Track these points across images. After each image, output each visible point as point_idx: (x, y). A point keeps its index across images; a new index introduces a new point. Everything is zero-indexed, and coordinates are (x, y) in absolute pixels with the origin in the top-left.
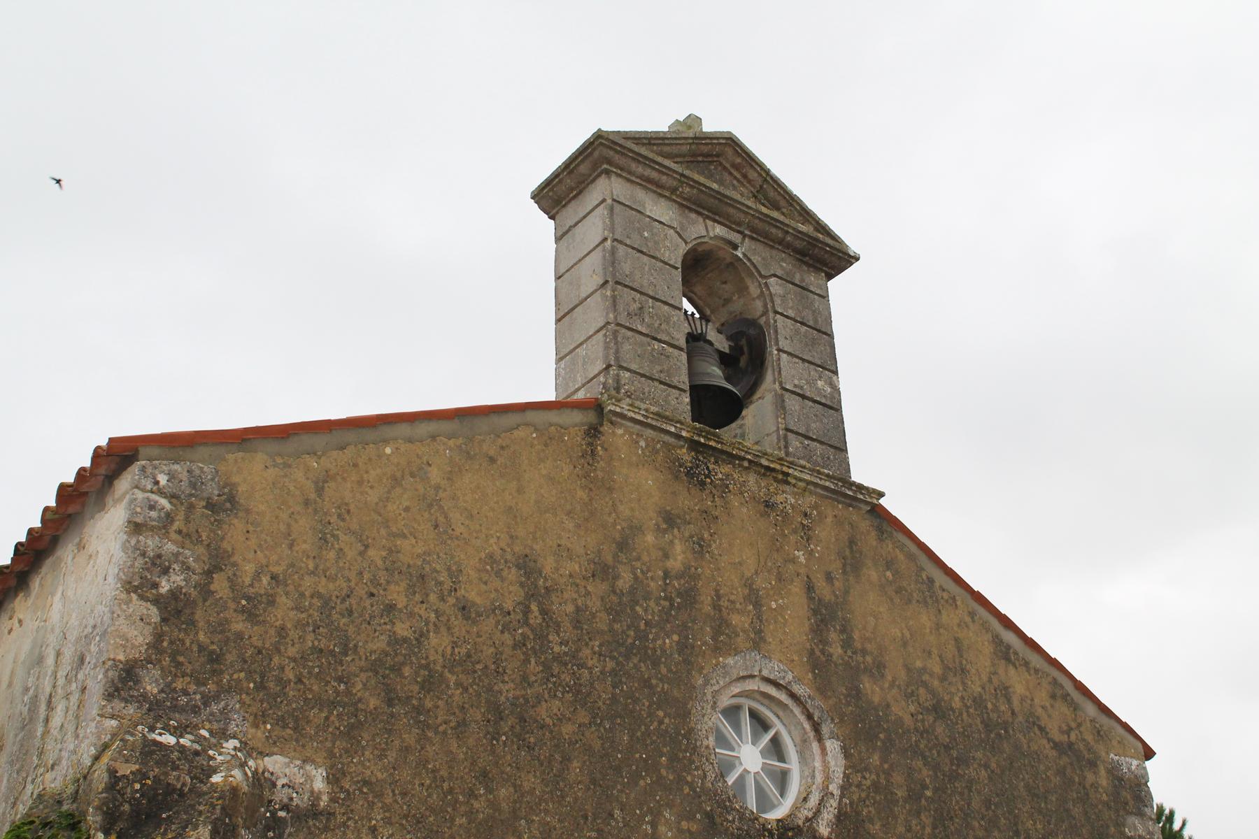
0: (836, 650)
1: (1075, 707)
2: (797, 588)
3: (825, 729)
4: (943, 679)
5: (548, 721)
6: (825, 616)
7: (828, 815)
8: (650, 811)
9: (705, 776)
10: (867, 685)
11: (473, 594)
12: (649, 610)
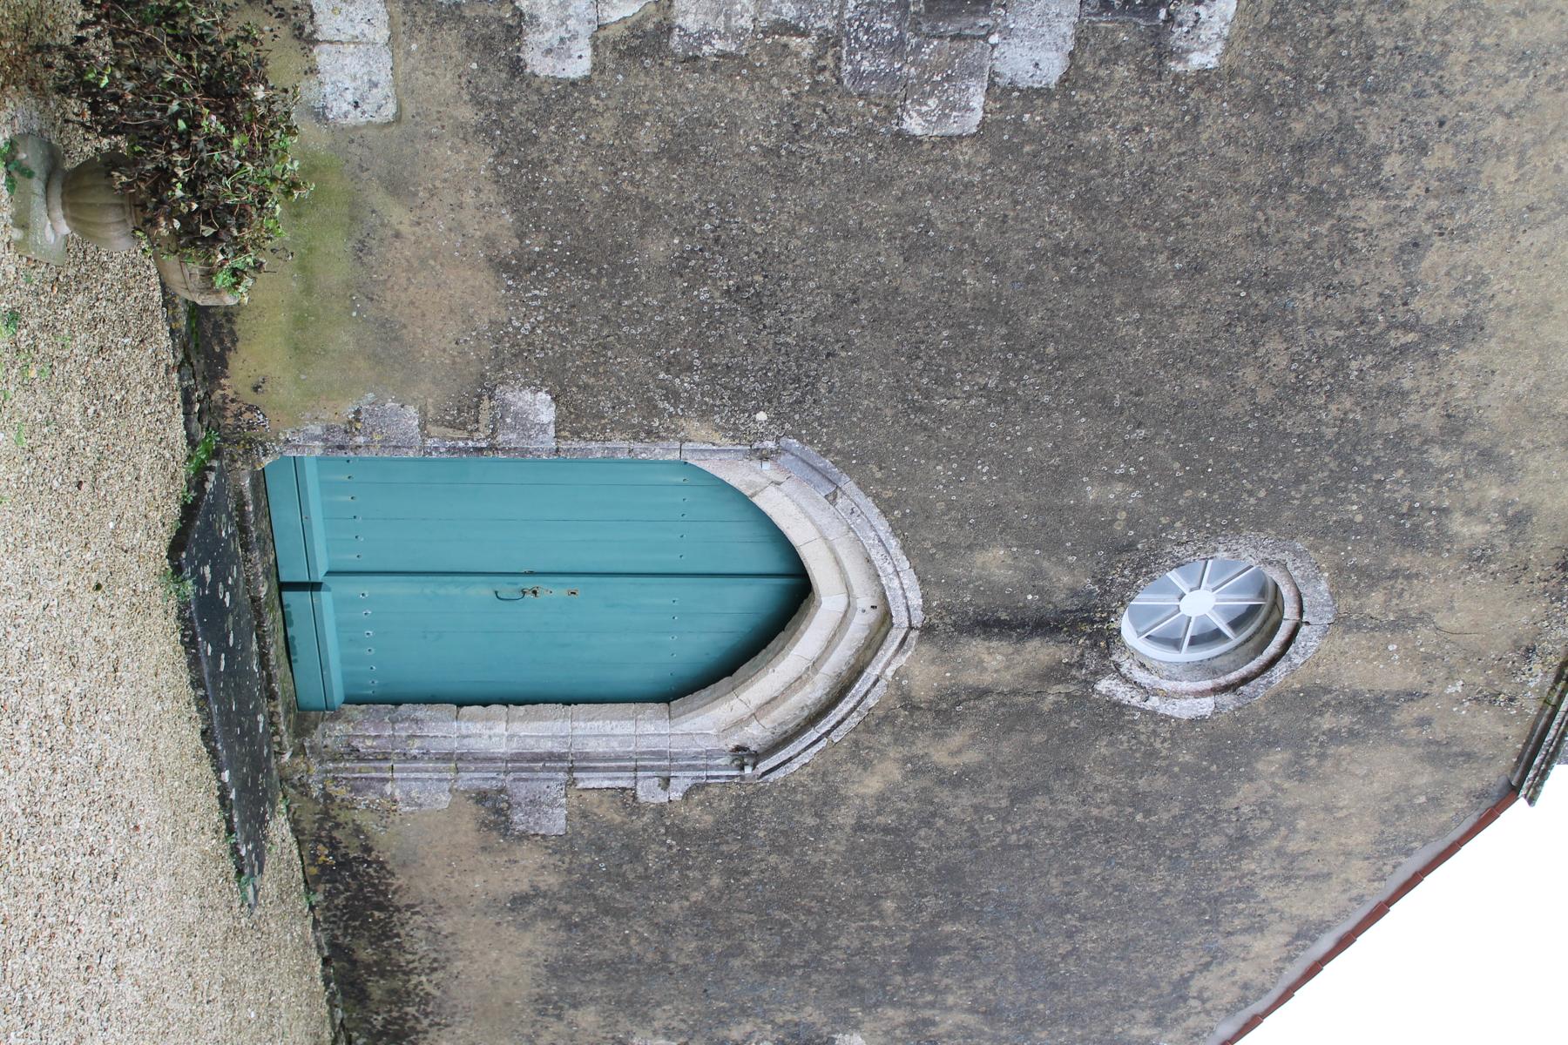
0: (1327, 722)
1: (1230, 1011)
2: (1412, 679)
3: (1227, 699)
4: (1280, 852)
6: (1373, 712)
7: (1122, 692)
8: (1141, 474)
10: (1279, 756)
11: (1434, 258)
12: (1398, 486)
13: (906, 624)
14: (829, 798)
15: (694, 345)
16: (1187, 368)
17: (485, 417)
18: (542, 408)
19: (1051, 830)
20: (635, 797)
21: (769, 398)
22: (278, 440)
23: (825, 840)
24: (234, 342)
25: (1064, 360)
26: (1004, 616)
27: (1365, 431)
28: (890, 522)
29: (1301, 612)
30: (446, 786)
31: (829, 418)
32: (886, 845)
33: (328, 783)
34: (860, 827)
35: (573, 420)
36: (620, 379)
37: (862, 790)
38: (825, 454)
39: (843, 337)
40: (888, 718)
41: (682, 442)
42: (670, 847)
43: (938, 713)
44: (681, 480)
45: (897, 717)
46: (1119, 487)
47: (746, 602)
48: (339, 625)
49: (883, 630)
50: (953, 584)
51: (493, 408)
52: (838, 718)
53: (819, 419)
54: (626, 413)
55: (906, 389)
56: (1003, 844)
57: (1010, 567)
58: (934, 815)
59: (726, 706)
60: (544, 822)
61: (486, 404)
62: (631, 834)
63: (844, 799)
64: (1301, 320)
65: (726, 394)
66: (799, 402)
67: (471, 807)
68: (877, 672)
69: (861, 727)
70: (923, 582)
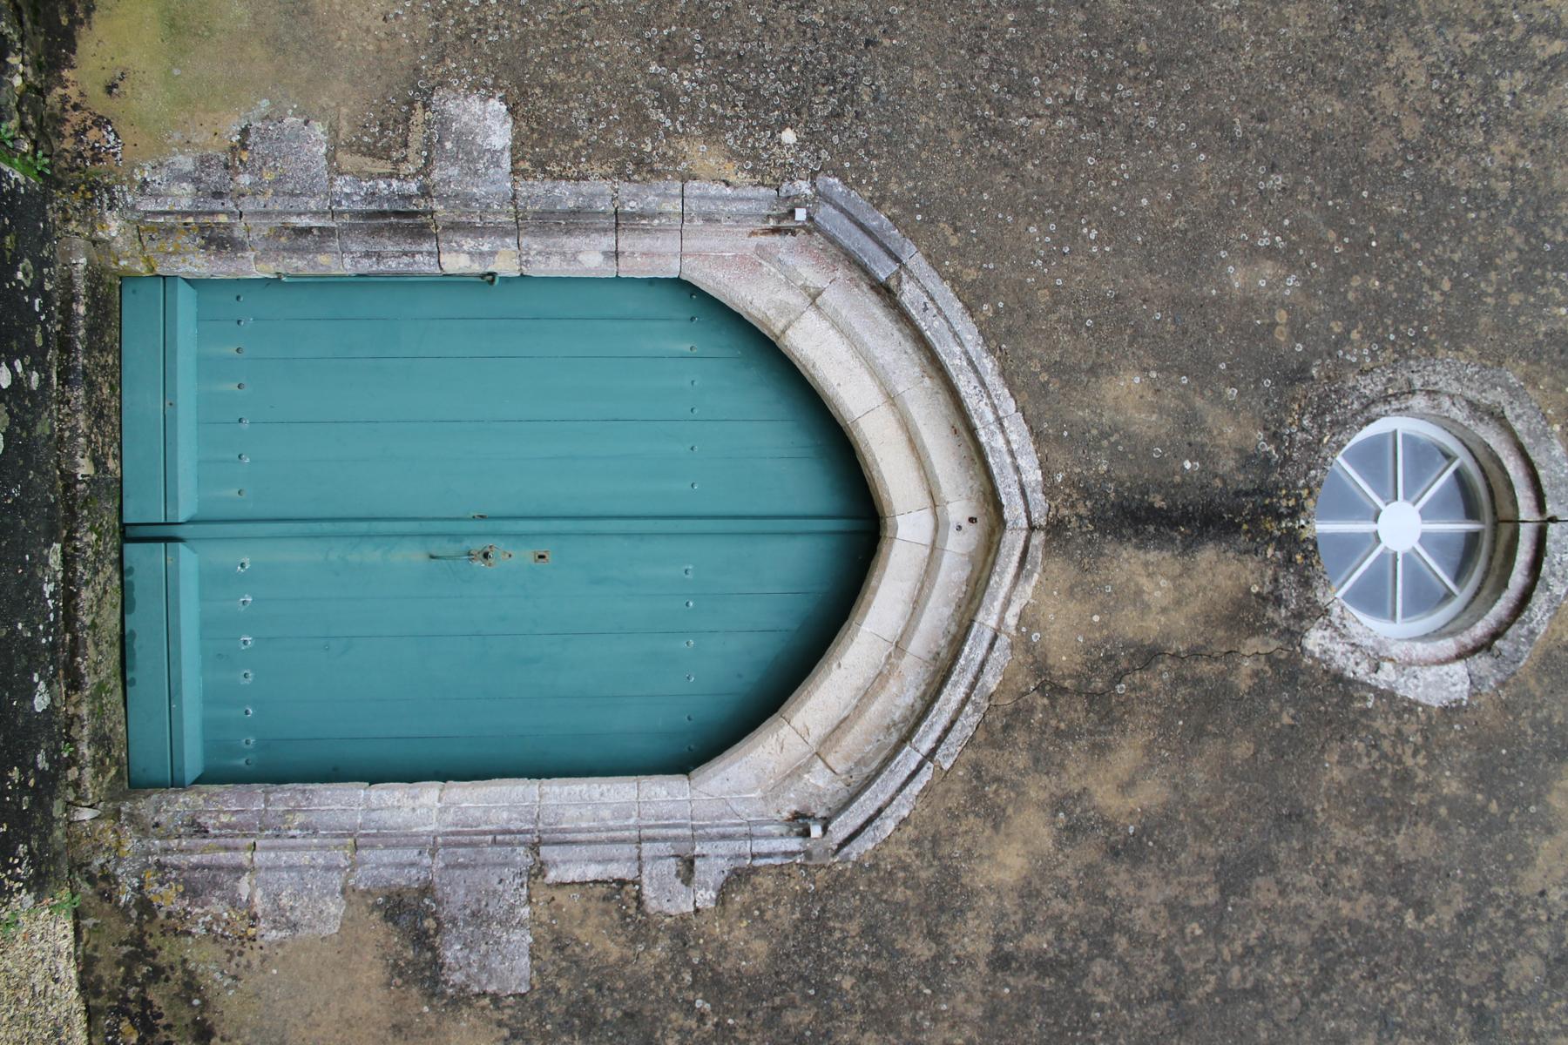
3: (1482, 663)
5: (1392, 61)
8: (1292, 248)
9: (1363, 372)
13: (1023, 523)
14: (946, 898)
15: (693, 23)
16: (1310, 81)
17: (416, 139)
18: (492, 124)
19: (1289, 951)
20: (639, 899)
21: (797, 108)
22: (132, 180)
23: (949, 994)
24: (89, 10)
25: (1165, 62)
26: (1159, 502)
27: (1543, 189)
28: (978, 324)
29: (1541, 505)
30: (337, 880)
31: (878, 144)
32: (1044, 998)
33: (149, 876)
34: (1001, 962)
35: (539, 147)
36: (598, 74)
37: (997, 876)
38: (877, 203)
39: (883, 18)
40: (1018, 715)
41: (684, 181)
42: (702, 1018)
43: (1091, 696)
44: (685, 347)
45: (1031, 710)
46: (1268, 268)
47: (791, 566)
48: (205, 625)
49: (990, 559)
50: (1082, 440)
51: (427, 123)
52: (944, 721)
53: (865, 144)
54: (607, 130)
55: (971, 100)
56: (1221, 988)
57: (1152, 408)
58: (1110, 926)
59: (772, 741)
60: (495, 962)
61: (419, 116)
62: (638, 985)
63: (972, 894)
64: (1426, 17)
65: (740, 98)
66: (837, 115)
67: (375, 930)
68: (992, 622)
69: (981, 737)
70: (1037, 436)
